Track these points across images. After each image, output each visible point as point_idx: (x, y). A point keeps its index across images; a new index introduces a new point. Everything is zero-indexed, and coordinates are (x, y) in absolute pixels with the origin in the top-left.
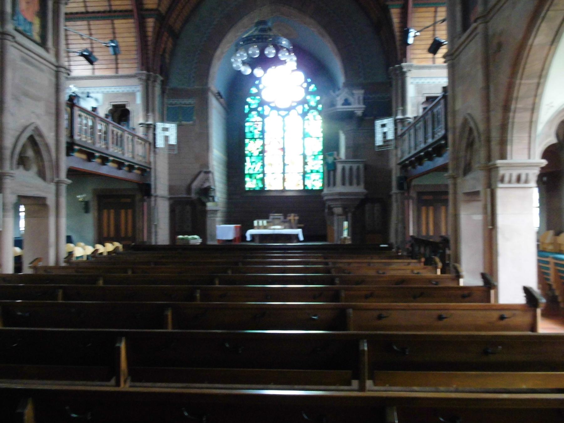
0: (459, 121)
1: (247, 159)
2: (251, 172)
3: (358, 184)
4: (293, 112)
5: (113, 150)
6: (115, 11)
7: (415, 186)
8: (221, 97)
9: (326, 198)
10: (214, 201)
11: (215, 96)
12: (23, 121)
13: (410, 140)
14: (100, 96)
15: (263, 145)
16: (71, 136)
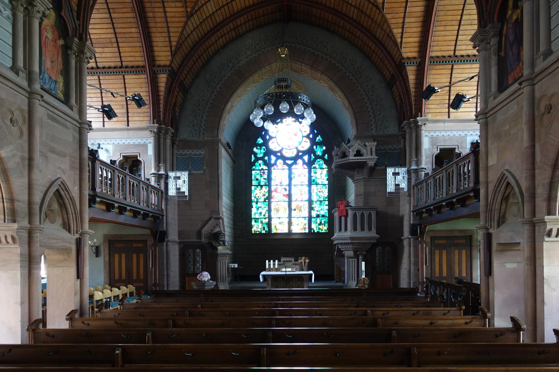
0: (493, 177)
1: (254, 204)
2: (257, 216)
3: (370, 229)
4: (300, 161)
5: (130, 201)
6: (127, 67)
7: (429, 231)
8: (230, 148)
9: (335, 242)
10: (224, 244)
11: (224, 147)
12: (77, 188)
13: (427, 189)
14: (110, 148)
15: (270, 192)
16: (93, 188)
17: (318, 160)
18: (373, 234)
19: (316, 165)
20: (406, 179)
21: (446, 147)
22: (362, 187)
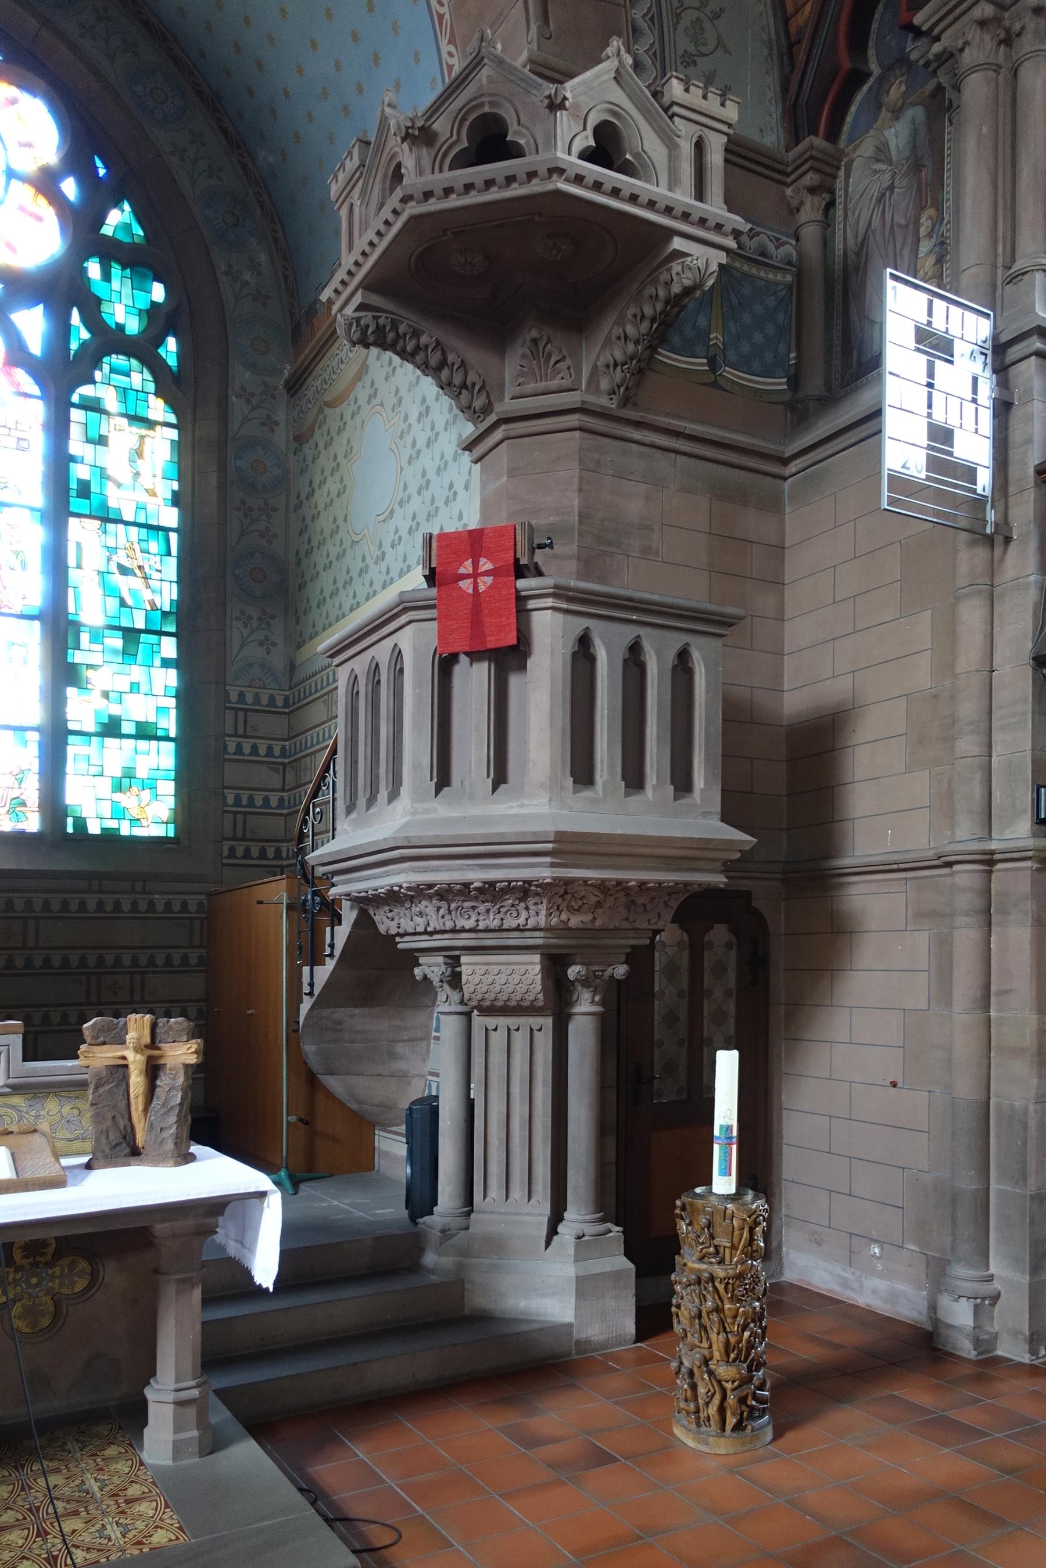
17: (119, 360)
18: (698, 819)
19: (101, 389)
22: (570, 472)
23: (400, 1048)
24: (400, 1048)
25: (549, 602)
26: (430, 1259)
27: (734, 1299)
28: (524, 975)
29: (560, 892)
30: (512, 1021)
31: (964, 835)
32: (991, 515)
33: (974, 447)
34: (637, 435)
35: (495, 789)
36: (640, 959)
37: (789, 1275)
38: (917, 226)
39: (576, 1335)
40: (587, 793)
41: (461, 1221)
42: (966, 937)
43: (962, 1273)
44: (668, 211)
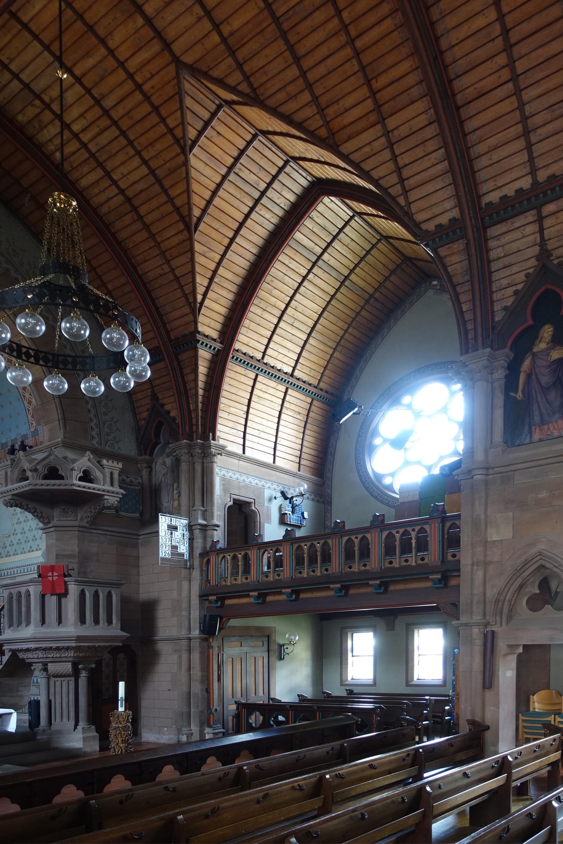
18: (115, 630)
20: (186, 540)
21: (242, 498)
23: (20, 688)
24: (20, 688)
25: (73, 583)
26: (39, 737)
27: (124, 731)
28: (68, 667)
29: (77, 649)
30: (62, 679)
31: (184, 633)
32: (188, 564)
33: (183, 549)
34: (95, 531)
35: (59, 625)
36: (99, 663)
37: (143, 740)
38: (173, 486)
39: (83, 750)
40: (84, 626)
41: (49, 728)
42: (185, 656)
43: (185, 730)
44: (103, 491)
